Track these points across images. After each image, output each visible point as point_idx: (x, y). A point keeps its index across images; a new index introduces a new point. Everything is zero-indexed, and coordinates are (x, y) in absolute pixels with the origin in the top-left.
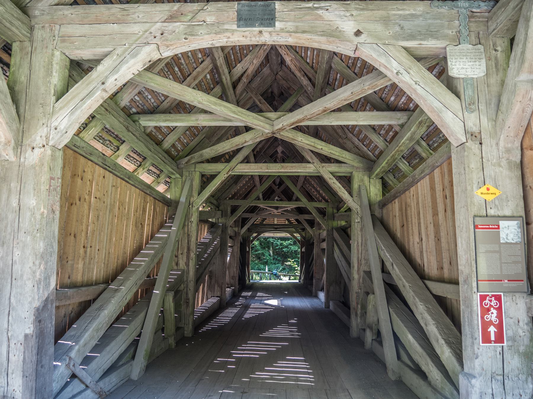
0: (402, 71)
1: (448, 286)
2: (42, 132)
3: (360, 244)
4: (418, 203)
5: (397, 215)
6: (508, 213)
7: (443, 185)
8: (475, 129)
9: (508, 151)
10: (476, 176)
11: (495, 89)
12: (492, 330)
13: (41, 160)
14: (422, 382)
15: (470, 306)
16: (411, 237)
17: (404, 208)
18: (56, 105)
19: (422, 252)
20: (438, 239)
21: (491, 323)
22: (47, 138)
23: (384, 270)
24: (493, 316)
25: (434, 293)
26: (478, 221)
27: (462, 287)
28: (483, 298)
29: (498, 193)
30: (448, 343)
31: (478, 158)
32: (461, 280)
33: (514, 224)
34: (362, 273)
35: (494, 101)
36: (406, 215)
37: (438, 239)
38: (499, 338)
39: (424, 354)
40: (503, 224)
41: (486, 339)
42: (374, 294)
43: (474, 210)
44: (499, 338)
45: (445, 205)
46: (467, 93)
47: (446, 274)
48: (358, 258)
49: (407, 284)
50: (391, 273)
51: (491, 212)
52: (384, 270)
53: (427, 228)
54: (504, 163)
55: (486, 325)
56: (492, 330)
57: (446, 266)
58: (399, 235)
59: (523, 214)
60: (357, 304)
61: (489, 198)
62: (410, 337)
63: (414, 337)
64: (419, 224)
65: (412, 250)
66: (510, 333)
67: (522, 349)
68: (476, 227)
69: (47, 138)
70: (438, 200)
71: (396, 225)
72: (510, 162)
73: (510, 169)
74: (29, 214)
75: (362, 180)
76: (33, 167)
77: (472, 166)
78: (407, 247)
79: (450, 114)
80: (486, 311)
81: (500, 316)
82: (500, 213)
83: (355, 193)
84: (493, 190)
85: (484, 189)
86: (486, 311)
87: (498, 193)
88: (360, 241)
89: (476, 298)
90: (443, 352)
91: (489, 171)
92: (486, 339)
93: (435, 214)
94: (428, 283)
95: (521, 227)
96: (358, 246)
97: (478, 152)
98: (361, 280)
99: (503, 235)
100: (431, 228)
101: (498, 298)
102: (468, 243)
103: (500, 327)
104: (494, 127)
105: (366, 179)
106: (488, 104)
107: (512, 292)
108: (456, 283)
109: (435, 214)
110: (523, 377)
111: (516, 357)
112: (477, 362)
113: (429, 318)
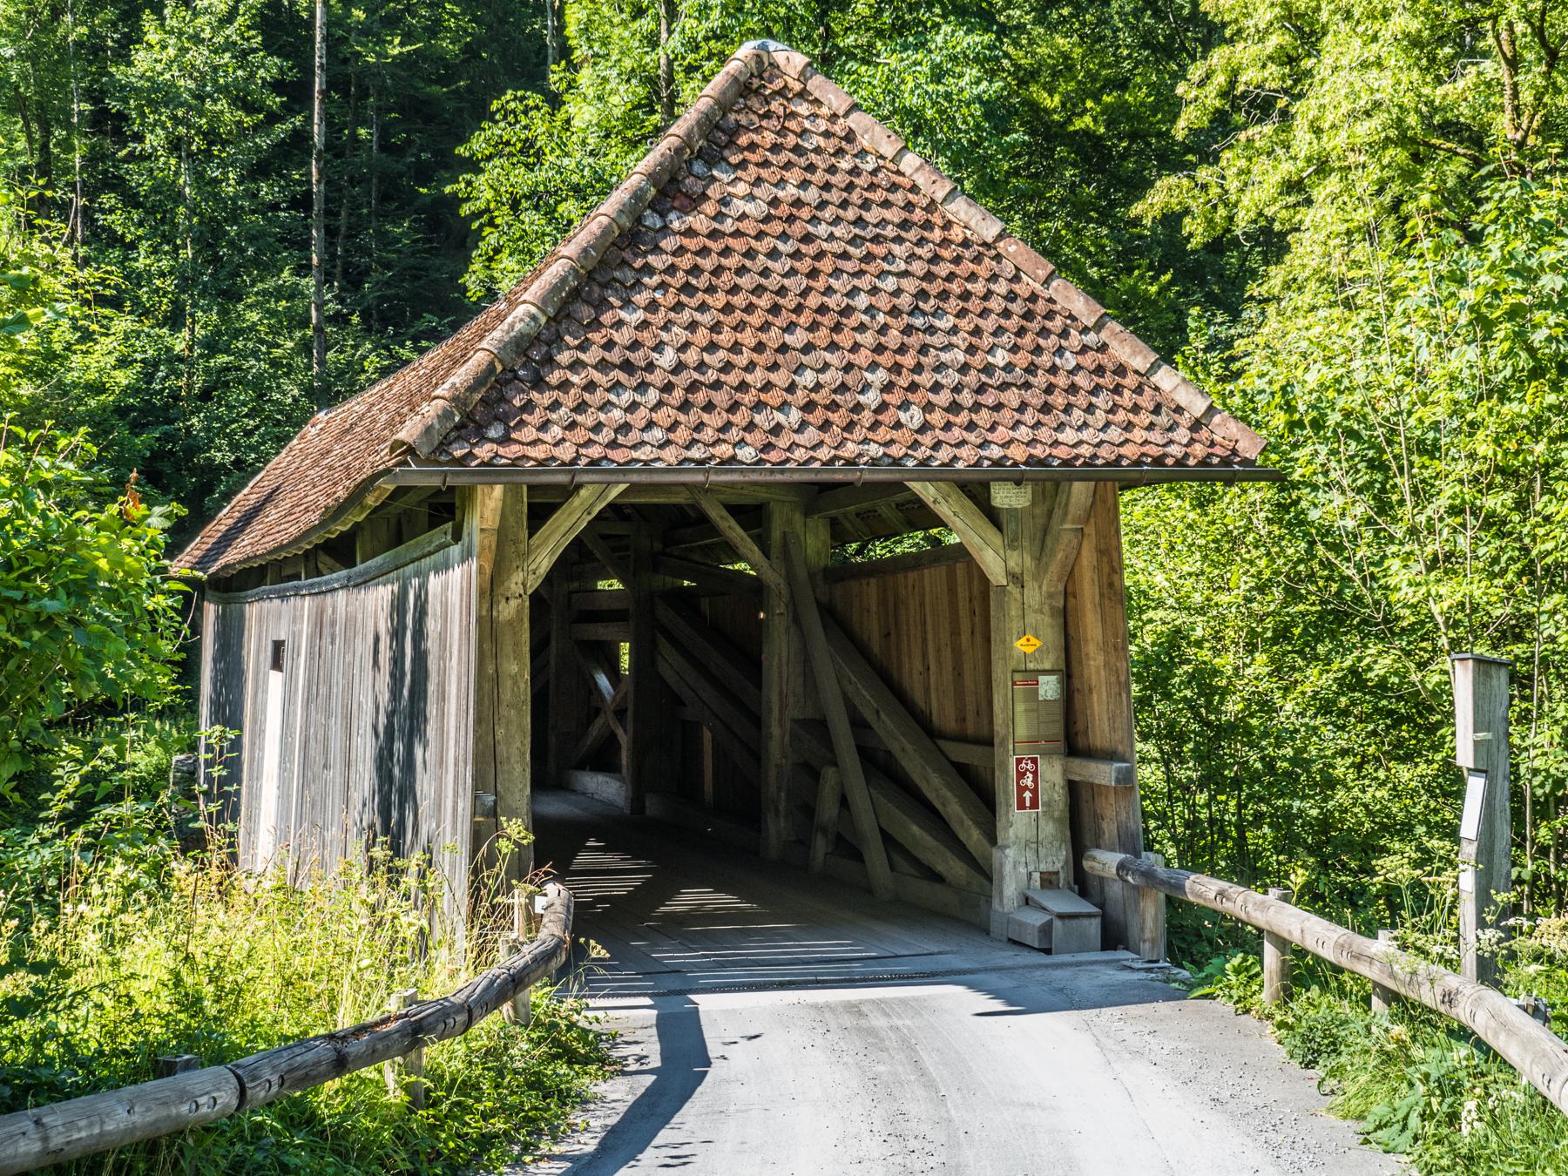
0: (940, 499)
1: (974, 748)
2: (518, 577)
3: (784, 660)
4: (922, 604)
5: (874, 609)
6: (1047, 666)
7: (971, 593)
8: (1017, 570)
9: (1051, 596)
10: (1015, 626)
11: (1040, 521)
12: (1027, 795)
13: (519, 611)
14: (937, 887)
15: (1005, 770)
16: (905, 660)
17: (891, 604)
18: (532, 541)
19: (927, 690)
20: (958, 673)
21: (1026, 788)
22: (524, 584)
23: (859, 724)
24: (1028, 781)
25: (954, 759)
26: (1017, 677)
27: (997, 750)
28: (1019, 761)
29: (1039, 644)
30: (977, 824)
31: (1019, 605)
32: (997, 741)
33: (1053, 678)
34: (788, 725)
35: (1039, 534)
36: (896, 617)
37: (958, 673)
38: (1034, 805)
39: (942, 848)
40: (1042, 679)
41: (1021, 806)
42: (836, 764)
43: (1013, 664)
44: (1034, 805)
45: (973, 625)
46: (1010, 527)
47: (970, 728)
48: (781, 693)
49: (909, 747)
50: (875, 726)
51: (1031, 666)
52: (859, 724)
53: (938, 650)
54: (1046, 609)
55: (1021, 790)
56: (1027, 795)
57: (970, 717)
58: (876, 649)
59: (1063, 667)
60: (779, 789)
61: (1029, 650)
62: (915, 829)
63: (921, 828)
64: (925, 640)
65: (906, 683)
66: (1046, 798)
67: (1056, 814)
68: (1014, 683)
69: (524, 584)
70: (961, 612)
71: (871, 629)
72: (1052, 608)
73: (1052, 616)
74: (509, 683)
75: (790, 522)
76: (510, 623)
77: (1013, 613)
78: (895, 674)
79: (991, 552)
80: (1021, 775)
81: (1035, 781)
82: (1040, 667)
83: (775, 552)
84: (1033, 640)
85: (1023, 641)
86: (1021, 775)
87: (1039, 644)
88: (784, 654)
89: (1013, 761)
90: (970, 836)
91: (1031, 618)
92: (1021, 806)
93: (955, 632)
94: (942, 744)
95: (1060, 682)
96: (780, 666)
97: (1018, 596)
98: (787, 738)
99: (1041, 692)
100: (947, 654)
101: (1034, 761)
102: (1006, 701)
103: (1035, 792)
104: (1037, 566)
105: (798, 517)
106: (1032, 540)
107: (1047, 754)
108: (989, 742)
109: (955, 632)
110: (1056, 844)
111: (1050, 824)
112: (1011, 831)
113: (949, 794)
